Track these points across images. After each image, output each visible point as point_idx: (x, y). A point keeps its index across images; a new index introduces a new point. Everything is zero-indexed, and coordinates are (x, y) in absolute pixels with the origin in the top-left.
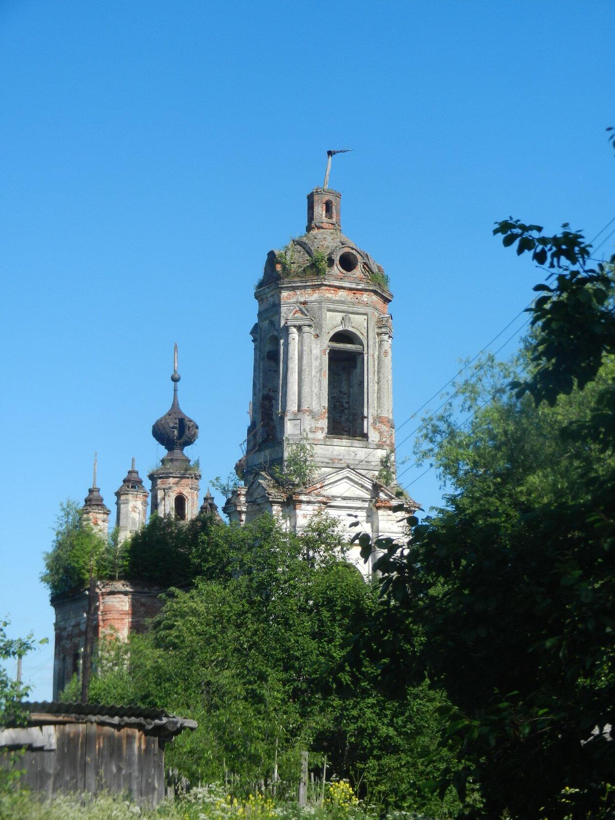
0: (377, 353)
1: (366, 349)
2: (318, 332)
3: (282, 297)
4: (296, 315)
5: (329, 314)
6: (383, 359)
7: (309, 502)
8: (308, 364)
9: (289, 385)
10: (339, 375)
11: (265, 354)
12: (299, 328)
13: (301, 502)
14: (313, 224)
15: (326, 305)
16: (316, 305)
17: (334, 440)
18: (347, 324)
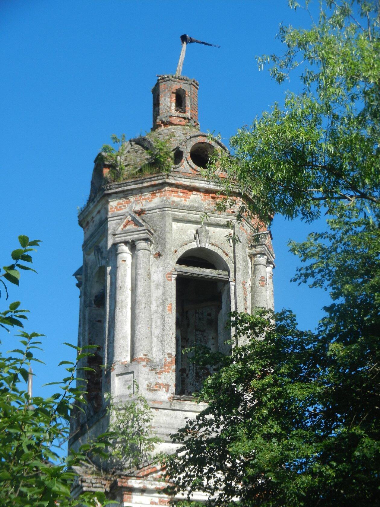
0: (249, 283)
1: (232, 274)
2: (159, 249)
3: (109, 207)
4: (128, 227)
5: (175, 225)
6: (258, 290)
7: (143, 491)
8: (145, 293)
9: (118, 326)
10: (203, 331)
11: (93, 298)
12: (133, 246)
13: (131, 490)
14: (158, 121)
15: (170, 213)
16: (158, 212)
17: (186, 402)
18: (203, 239)
